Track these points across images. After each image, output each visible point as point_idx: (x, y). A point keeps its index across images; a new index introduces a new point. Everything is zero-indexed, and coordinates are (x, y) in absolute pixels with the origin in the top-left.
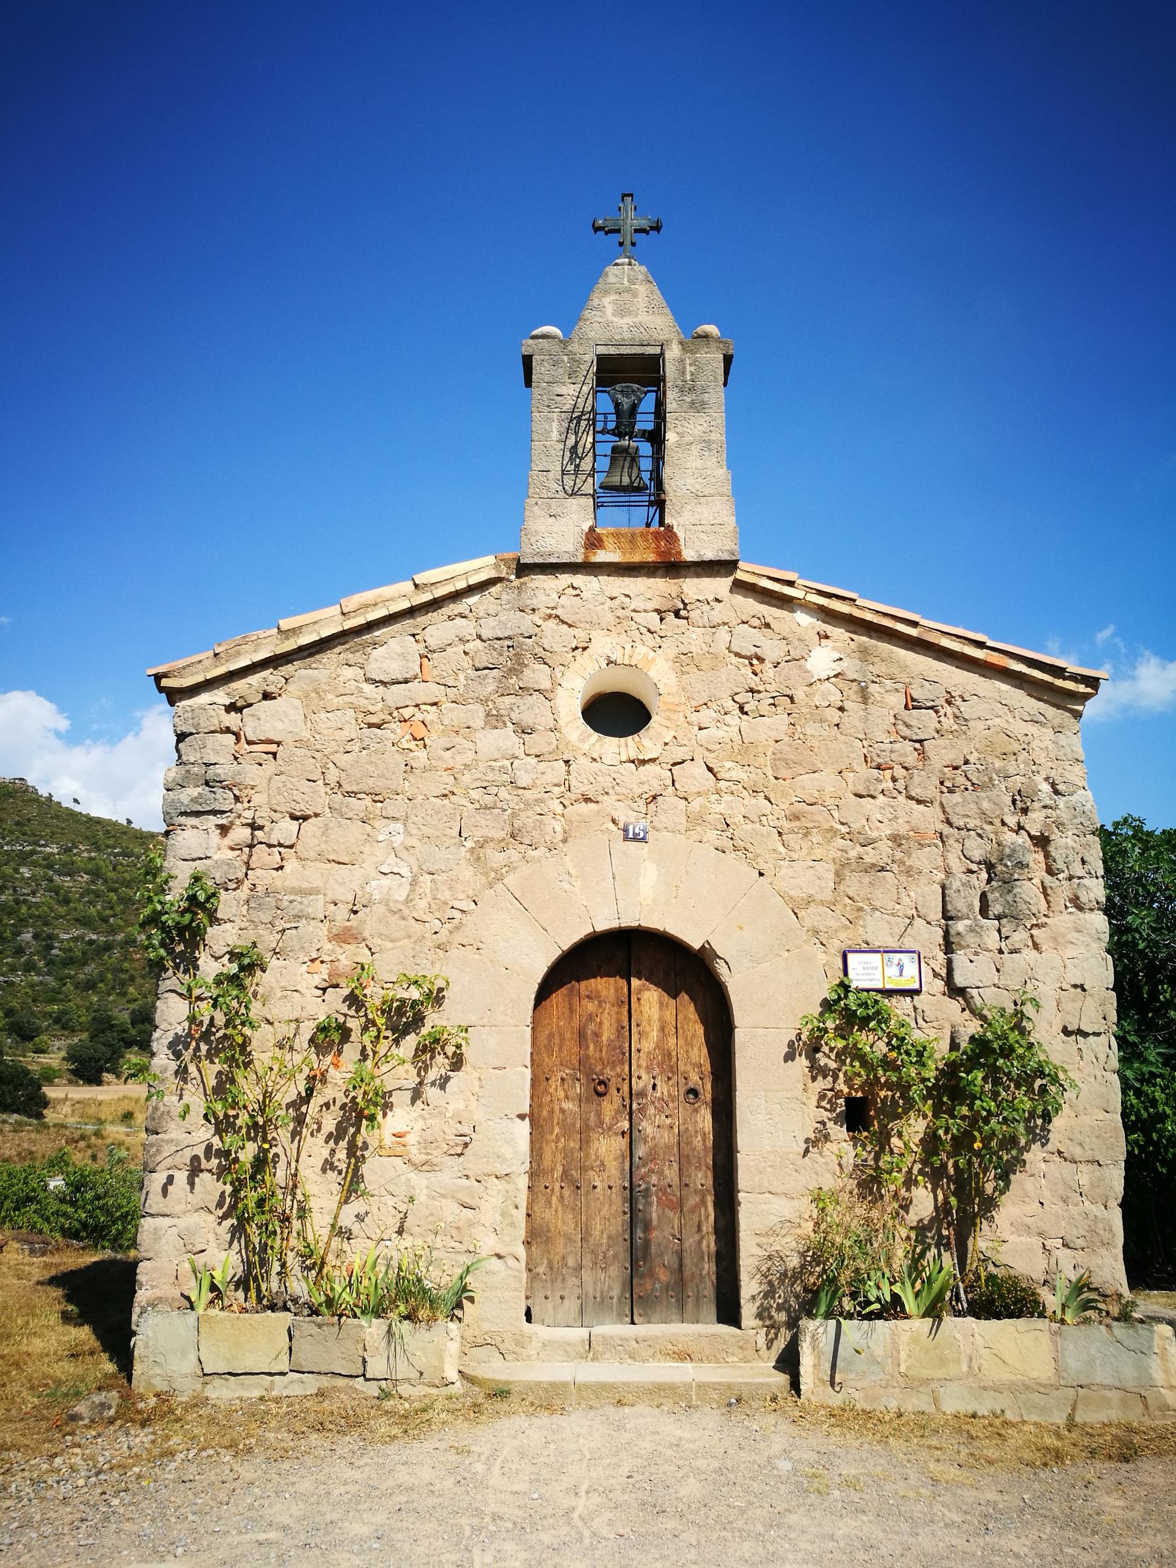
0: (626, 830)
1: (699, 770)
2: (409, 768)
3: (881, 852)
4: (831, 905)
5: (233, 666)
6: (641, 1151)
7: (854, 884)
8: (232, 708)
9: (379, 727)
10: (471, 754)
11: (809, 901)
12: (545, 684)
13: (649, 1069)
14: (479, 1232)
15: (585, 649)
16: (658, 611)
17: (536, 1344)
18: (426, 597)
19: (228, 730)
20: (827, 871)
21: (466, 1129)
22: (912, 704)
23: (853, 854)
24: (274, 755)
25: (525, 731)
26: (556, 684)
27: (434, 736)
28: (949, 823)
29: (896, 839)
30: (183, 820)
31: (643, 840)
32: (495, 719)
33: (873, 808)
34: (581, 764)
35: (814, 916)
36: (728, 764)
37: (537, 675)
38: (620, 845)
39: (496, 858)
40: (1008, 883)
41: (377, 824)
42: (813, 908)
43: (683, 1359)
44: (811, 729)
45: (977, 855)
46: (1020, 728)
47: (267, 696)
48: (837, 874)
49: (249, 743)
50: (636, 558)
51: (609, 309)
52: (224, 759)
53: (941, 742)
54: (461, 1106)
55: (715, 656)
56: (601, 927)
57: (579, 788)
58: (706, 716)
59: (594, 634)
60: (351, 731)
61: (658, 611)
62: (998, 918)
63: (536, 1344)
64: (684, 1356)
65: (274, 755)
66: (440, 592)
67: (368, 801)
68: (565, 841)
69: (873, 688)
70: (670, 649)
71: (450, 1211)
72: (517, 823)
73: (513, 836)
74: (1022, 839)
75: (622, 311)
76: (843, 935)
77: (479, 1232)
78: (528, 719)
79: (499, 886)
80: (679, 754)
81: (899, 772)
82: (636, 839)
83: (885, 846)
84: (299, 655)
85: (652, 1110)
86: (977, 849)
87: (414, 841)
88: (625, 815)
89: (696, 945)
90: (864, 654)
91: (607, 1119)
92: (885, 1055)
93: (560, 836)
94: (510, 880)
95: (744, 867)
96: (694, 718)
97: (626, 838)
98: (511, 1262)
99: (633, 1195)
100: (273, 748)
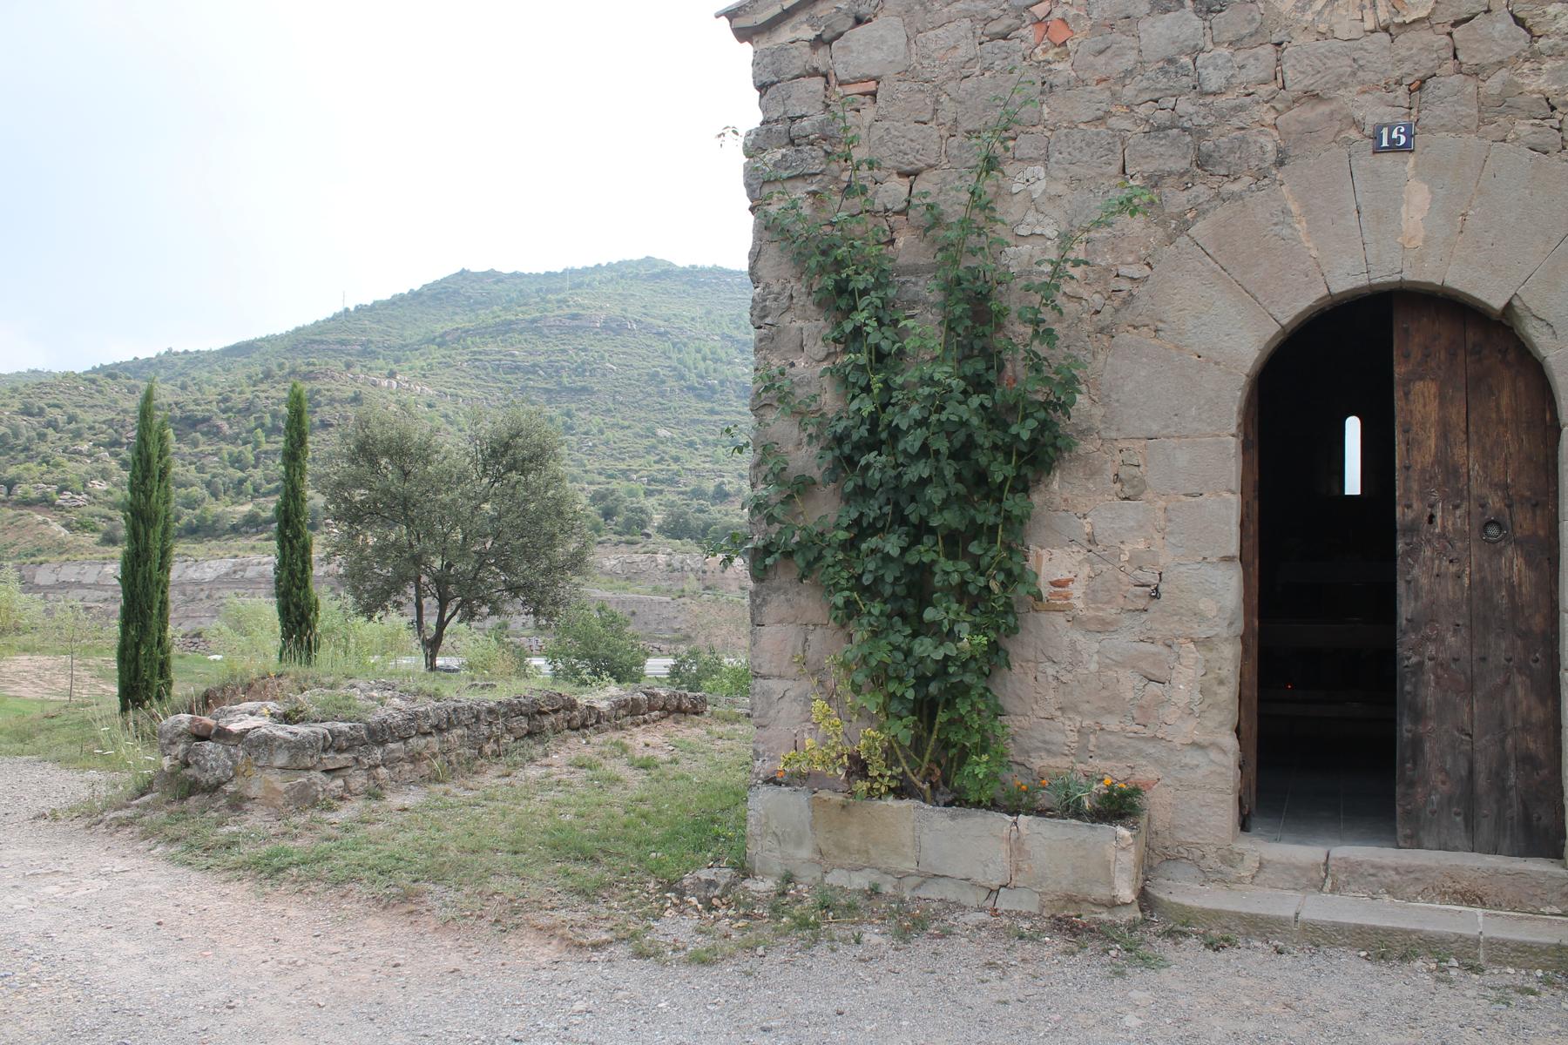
0: (1377, 137)
2: (1048, 88)
8: (818, 42)
9: (1005, 38)
17: (1251, 863)
19: (815, 72)
27: (1079, 37)
31: (1407, 148)
38: (1366, 160)
47: (859, 21)
49: (841, 84)
54: (1141, 546)
57: (1297, 80)
71: (1129, 684)
77: (1170, 714)
79: (1182, 241)
82: (1394, 147)
85: (1427, 552)
87: (1059, 188)
93: (1271, 157)
94: (1199, 229)
100: (871, 86)
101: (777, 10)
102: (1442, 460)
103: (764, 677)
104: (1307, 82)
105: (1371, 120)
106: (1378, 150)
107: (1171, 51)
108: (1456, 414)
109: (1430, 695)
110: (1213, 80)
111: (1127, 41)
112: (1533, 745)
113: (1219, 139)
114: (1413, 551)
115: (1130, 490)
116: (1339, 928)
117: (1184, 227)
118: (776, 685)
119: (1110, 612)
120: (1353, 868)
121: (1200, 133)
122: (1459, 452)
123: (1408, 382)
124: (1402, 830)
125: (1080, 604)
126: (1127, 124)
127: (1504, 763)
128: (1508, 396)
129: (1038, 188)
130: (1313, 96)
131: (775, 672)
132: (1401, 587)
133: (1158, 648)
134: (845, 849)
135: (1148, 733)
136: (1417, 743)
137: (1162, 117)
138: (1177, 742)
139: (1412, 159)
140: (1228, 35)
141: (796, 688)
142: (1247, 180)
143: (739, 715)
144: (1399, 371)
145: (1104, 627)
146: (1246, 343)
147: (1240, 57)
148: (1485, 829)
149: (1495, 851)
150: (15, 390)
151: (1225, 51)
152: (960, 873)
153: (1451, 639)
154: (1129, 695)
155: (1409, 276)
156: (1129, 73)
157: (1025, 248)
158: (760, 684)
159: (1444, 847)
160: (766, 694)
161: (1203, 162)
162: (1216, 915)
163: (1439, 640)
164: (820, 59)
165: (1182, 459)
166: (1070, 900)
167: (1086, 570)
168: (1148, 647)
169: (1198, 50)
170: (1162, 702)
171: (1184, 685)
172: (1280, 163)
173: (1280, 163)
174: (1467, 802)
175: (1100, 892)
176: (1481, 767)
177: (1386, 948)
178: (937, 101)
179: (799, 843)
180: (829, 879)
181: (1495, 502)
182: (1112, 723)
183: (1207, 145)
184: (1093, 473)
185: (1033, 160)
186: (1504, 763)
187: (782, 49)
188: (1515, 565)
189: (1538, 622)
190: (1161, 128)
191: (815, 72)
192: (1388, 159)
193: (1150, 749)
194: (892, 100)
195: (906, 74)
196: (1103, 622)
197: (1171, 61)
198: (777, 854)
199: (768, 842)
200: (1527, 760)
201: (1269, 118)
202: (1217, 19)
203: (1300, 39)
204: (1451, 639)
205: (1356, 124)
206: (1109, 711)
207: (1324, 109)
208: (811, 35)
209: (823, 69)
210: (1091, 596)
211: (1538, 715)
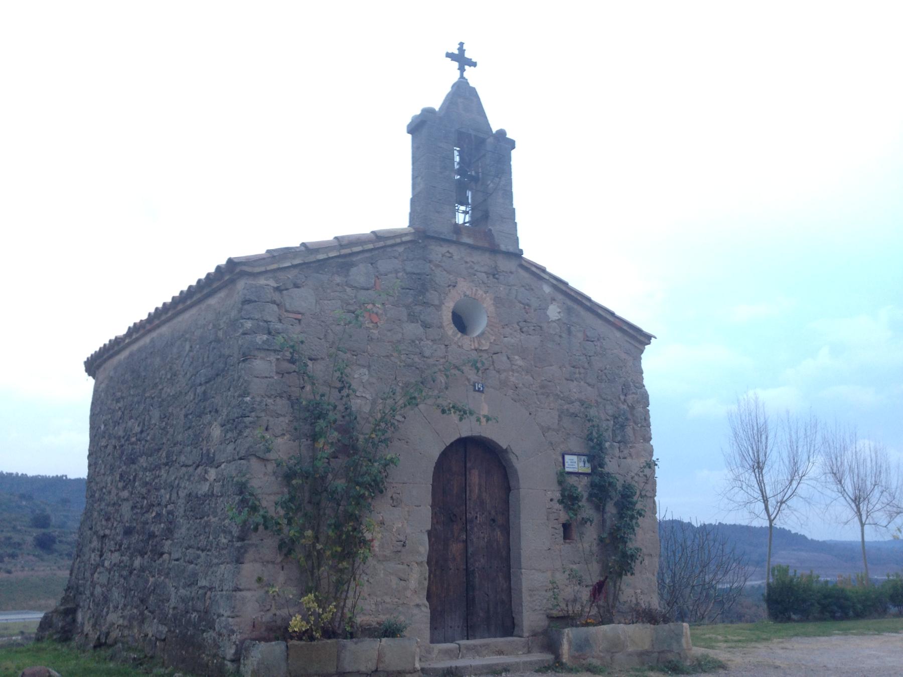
1: (505, 359)
6: (470, 550)
8: (277, 289)
10: (400, 335)
11: (549, 429)
12: (437, 302)
14: (408, 593)
17: (436, 651)
19: (274, 302)
21: (402, 538)
25: (426, 326)
26: (442, 303)
30: (256, 353)
31: (482, 392)
33: (573, 385)
36: (517, 357)
40: (623, 427)
41: (354, 368)
43: (500, 654)
45: (610, 412)
47: (296, 286)
48: (559, 416)
49: (286, 311)
62: (619, 442)
63: (436, 651)
64: (500, 653)
65: (300, 320)
67: (349, 355)
68: (447, 388)
71: (394, 581)
72: (424, 375)
76: (562, 446)
82: (479, 391)
84: (611, 319)
85: (476, 529)
87: (374, 380)
90: (569, 311)
91: (456, 535)
98: (423, 609)
99: (468, 573)
100: (299, 316)
105: (472, 380)
106: (475, 390)
118: (248, 594)
119: (387, 553)
125: (377, 549)
126: (396, 360)
129: (365, 378)
133: (405, 567)
137: (409, 361)
139: (483, 396)
141: (327, 616)
143: (300, 639)
147: (435, 347)
149: (495, 637)
150: (679, 654)
153: (482, 560)
155: (483, 435)
157: (359, 401)
159: (482, 637)
164: (277, 296)
169: (421, 340)
171: (413, 583)
185: (363, 366)
188: (498, 533)
190: (409, 366)
191: (274, 302)
192: (477, 394)
197: (413, 341)
204: (482, 560)
208: (276, 285)
209: (278, 302)
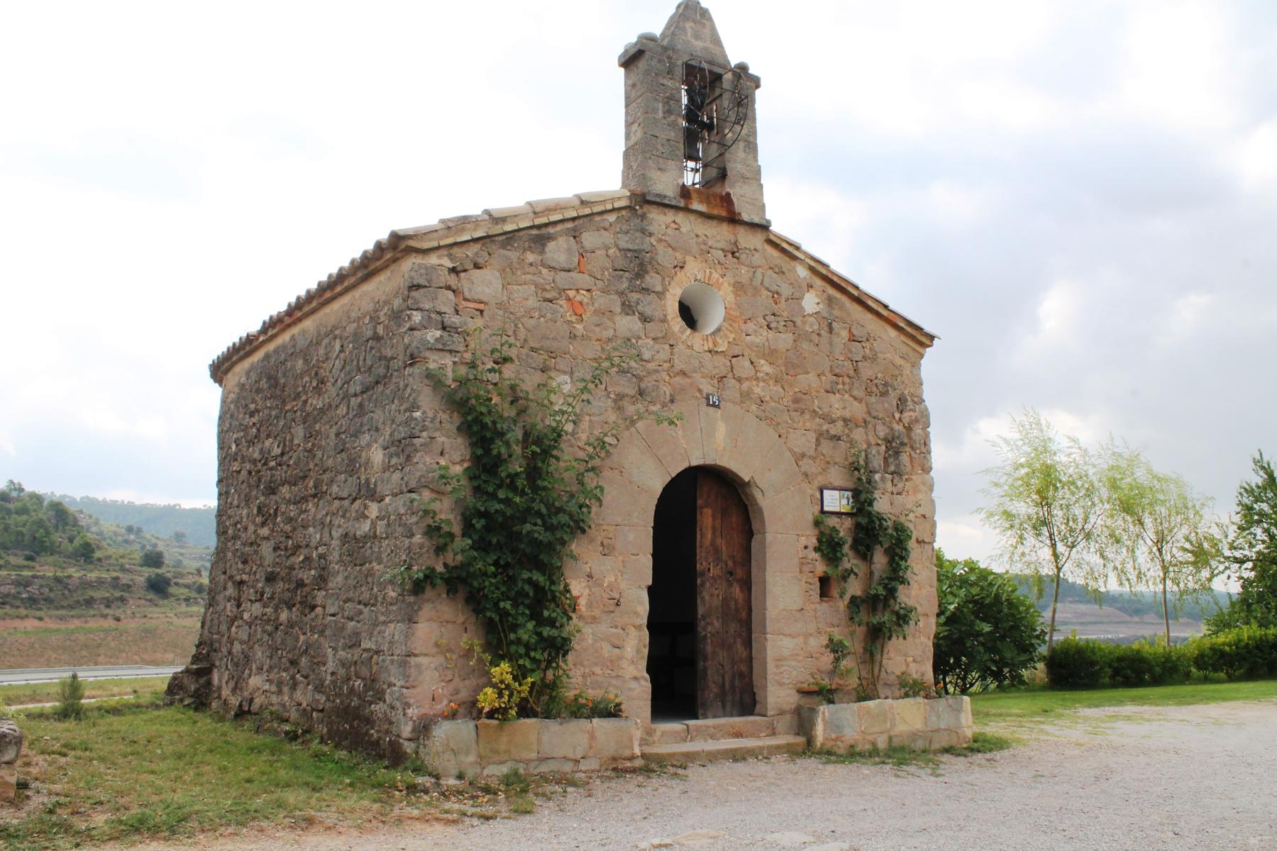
0: (708, 399)
2: (573, 337)
3: (837, 429)
4: (814, 459)
5: (459, 240)
7: (826, 447)
9: (551, 301)
11: (803, 455)
12: (659, 288)
13: (706, 559)
15: (682, 267)
16: (723, 250)
18: (587, 211)
20: (812, 436)
22: (853, 339)
23: (825, 428)
24: (482, 312)
25: (645, 319)
27: (588, 314)
28: (869, 413)
29: (845, 420)
30: (428, 354)
31: (718, 407)
32: (628, 308)
33: (834, 399)
34: (680, 347)
35: (807, 465)
36: (762, 362)
37: (653, 280)
38: (704, 408)
39: (631, 409)
42: (805, 460)
44: (805, 345)
46: (899, 361)
47: (477, 266)
50: (715, 212)
51: (689, 32)
52: (448, 309)
53: (866, 364)
54: (613, 579)
55: (755, 288)
56: (694, 463)
57: (679, 365)
58: (751, 326)
59: (688, 258)
60: (532, 302)
61: (723, 250)
62: (892, 473)
63: (658, 733)
64: (738, 735)
65: (482, 312)
66: (597, 209)
69: (834, 324)
70: (730, 278)
71: (607, 650)
73: (641, 394)
74: (901, 427)
75: (697, 37)
76: (820, 478)
77: (624, 663)
78: (648, 311)
79: (633, 429)
80: (736, 351)
81: (847, 380)
82: (714, 405)
83: (840, 423)
85: (708, 584)
86: (882, 431)
88: (707, 388)
89: (747, 480)
90: (830, 301)
92: (725, 601)
93: (668, 398)
94: (640, 425)
95: (771, 431)
96: (743, 326)
97: (708, 405)
100: (481, 306)
101: (436, 244)
102: (713, 544)
103: (416, 655)
104: (683, 367)
105: (705, 391)
106: (708, 405)
107: (629, 335)
108: (718, 522)
109: (709, 648)
110: (646, 356)
111: (610, 324)
112: (743, 668)
113: (647, 383)
114: (703, 584)
115: (607, 549)
116: (719, 752)
117: (633, 423)
119: (597, 613)
120: (698, 729)
121: (640, 379)
122: (719, 541)
123: (702, 508)
124: (700, 712)
125: (583, 609)
127: (734, 678)
128: (735, 519)
130: (683, 373)
131: (424, 651)
132: (699, 601)
133: (620, 631)
134: (497, 752)
135: (613, 674)
136: (705, 670)
138: (627, 677)
140: (652, 335)
142: (659, 406)
144: (699, 502)
145: (594, 620)
146: (657, 484)
147: (657, 347)
148: (729, 705)
149: (732, 715)
151: (651, 342)
152: (561, 753)
153: (716, 623)
154: (607, 655)
155: (718, 463)
156: (609, 340)
158: (413, 660)
159: (715, 717)
160: (418, 666)
161: (641, 393)
162: (672, 755)
163: (712, 624)
165: (631, 537)
166: (614, 759)
167: (587, 591)
168: (613, 630)
170: (620, 658)
172: (672, 401)
173: (672, 401)
174: (722, 696)
175: (627, 753)
176: (727, 679)
177: (737, 756)
178: (516, 326)
179: (467, 753)
180: (486, 772)
181: (730, 563)
182: (598, 670)
183: (643, 385)
184: (592, 541)
185: (565, 373)
186: (734, 678)
187: (433, 268)
188: (737, 591)
189: (744, 615)
192: (712, 409)
193: (614, 682)
194: (493, 318)
195: (500, 305)
196: (594, 618)
198: (453, 762)
199: (448, 755)
200: (741, 675)
201: (667, 378)
202: (648, 325)
203: (681, 346)
205: (700, 391)
206: (596, 664)
207: (688, 380)
208: (451, 265)
210: (590, 605)
211: (745, 654)
